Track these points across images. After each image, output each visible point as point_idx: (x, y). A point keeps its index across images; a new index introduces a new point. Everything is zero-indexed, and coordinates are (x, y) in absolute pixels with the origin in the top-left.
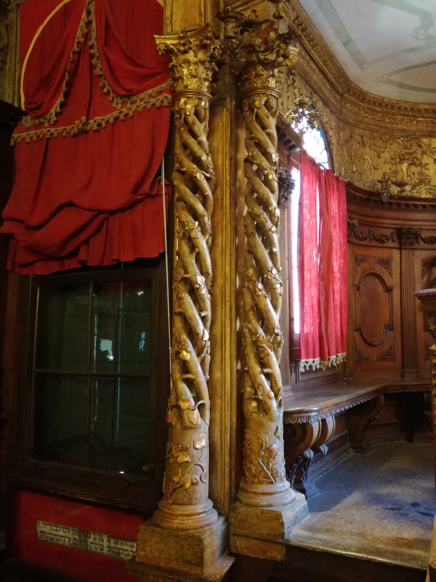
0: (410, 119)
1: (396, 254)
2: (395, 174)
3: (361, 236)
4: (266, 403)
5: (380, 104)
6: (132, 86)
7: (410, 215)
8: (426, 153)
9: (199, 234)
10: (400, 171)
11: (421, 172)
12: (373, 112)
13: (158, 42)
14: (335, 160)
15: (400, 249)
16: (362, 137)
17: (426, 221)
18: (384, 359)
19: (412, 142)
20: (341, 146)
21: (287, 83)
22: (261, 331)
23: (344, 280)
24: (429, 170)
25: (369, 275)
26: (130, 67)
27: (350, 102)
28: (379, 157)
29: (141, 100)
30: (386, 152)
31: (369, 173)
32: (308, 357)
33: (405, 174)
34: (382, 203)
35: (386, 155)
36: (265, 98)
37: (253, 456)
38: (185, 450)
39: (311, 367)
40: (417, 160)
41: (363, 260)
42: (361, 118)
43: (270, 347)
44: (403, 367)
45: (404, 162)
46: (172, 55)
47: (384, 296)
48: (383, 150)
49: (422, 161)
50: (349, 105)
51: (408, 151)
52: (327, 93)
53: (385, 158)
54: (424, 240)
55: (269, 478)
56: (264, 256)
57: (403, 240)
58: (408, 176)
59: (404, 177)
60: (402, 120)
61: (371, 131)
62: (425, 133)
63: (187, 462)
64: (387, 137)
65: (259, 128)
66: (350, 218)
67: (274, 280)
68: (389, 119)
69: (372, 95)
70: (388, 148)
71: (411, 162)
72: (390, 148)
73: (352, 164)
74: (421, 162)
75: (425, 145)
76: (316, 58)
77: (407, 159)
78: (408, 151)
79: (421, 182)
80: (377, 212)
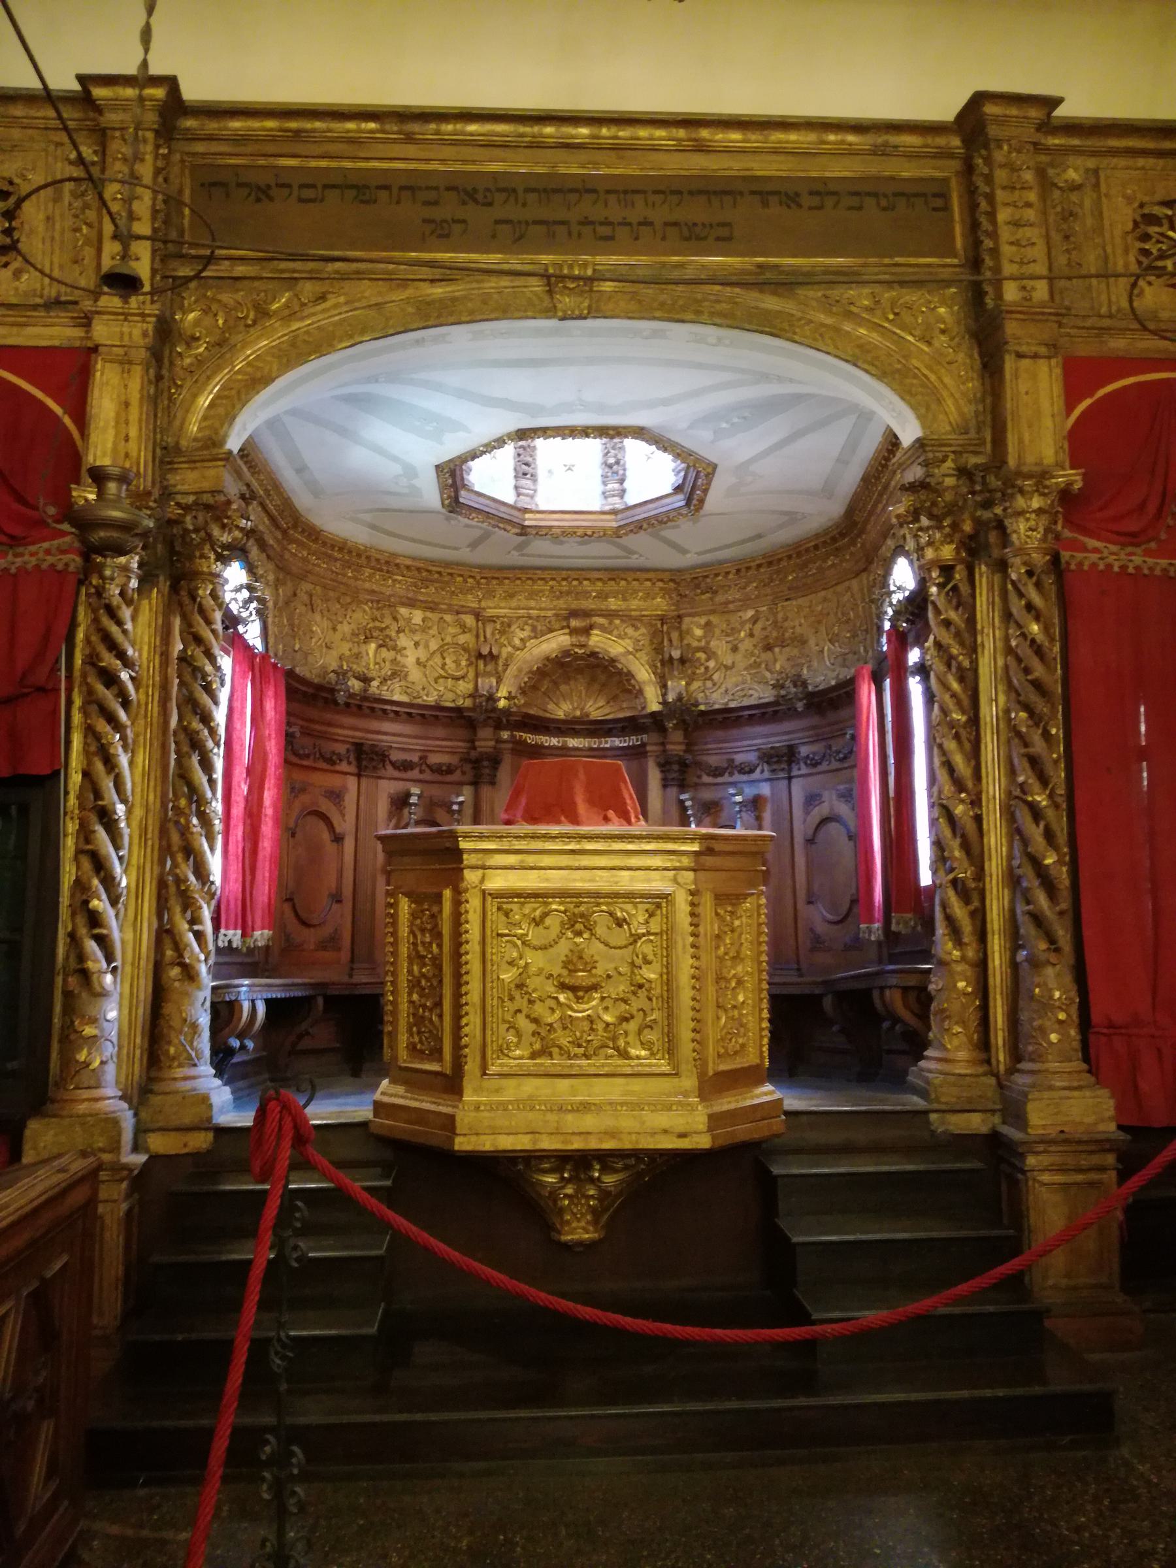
1: (352, 782)
3: (301, 752)
4: (193, 968)
5: (341, 549)
6: (18, 531)
7: (375, 725)
9: (120, 750)
10: (364, 654)
13: (74, 494)
14: (270, 633)
15: (359, 776)
17: (399, 735)
18: (325, 948)
20: (280, 610)
22: (192, 878)
23: (277, 821)
25: (310, 813)
26: (15, 506)
27: (296, 541)
28: (334, 629)
29: (32, 555)
31: (317, 654)
32: (227, 928)
33: (372, 660)
34: (336, 703)
35: (345, 628)
36: (211, 587)
37: (173, 1035)
38: (93, 1021)
41: (303, 790)
42: (310, 567)
43: (203, 898)
44: (352, 961)
47: (330, 848)
51: (377, 624)
54: (393, 764)
55: (192, 1059)
56: (202, 784)
57: (364, 763)
58: (376, 663)
60: (371, 576)
62: (404, 600)
63: (95, 1036)
64: (348, 600)
65: (201, 621)
66: (289, 724)
67: (212, 815)
73: (294, 637)
78: (377, 624)
79: (394, 674)
80: (328, 716)
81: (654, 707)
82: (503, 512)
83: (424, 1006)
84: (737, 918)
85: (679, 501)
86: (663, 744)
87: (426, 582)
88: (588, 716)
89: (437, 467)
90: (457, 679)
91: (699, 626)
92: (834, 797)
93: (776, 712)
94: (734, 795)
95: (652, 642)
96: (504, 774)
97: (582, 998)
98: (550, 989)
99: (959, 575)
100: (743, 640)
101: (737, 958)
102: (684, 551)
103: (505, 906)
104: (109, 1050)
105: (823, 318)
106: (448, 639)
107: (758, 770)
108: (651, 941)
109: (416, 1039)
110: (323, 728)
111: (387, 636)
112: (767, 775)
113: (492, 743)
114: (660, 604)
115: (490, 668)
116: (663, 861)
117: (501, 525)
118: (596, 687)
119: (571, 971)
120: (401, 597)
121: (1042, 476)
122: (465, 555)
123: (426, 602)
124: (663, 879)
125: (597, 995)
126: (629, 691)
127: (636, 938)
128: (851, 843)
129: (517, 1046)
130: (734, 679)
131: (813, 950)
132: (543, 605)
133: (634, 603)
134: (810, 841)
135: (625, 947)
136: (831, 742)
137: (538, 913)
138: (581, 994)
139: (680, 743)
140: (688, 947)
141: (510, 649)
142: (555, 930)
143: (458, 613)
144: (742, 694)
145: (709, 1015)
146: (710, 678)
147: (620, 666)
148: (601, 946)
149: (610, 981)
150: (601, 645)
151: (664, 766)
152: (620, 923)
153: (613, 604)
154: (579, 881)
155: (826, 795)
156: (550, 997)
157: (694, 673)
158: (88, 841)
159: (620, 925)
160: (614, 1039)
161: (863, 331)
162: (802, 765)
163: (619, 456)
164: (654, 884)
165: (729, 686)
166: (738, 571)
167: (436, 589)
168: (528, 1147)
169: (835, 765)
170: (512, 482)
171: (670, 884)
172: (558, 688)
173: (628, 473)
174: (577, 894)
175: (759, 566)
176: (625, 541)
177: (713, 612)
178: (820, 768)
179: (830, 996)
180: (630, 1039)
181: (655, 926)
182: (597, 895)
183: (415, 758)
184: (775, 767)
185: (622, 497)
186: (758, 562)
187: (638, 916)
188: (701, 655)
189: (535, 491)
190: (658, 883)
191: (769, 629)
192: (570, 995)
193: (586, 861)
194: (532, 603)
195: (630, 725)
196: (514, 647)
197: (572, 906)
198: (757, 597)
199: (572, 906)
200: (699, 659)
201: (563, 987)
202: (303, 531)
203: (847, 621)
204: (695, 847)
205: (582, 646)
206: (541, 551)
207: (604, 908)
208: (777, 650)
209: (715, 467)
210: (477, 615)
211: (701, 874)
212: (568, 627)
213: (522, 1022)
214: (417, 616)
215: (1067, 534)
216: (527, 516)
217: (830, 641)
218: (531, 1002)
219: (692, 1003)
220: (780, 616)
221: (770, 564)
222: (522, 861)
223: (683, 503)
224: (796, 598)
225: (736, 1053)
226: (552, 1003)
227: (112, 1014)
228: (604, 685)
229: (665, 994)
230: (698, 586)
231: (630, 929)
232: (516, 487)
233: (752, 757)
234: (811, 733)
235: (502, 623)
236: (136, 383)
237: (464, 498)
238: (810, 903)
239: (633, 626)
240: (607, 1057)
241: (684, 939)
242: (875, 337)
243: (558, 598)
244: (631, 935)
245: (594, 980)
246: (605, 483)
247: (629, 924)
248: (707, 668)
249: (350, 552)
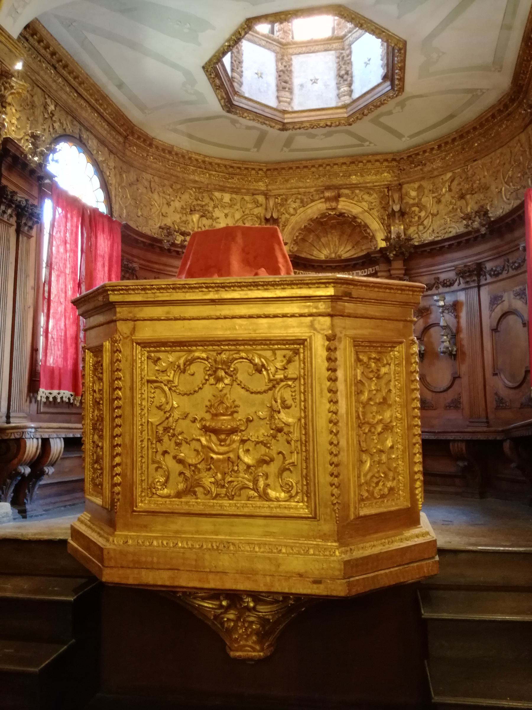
0: (202, 171)
2: (185, 223)
5: (170, 152)
8: (218, 207)
11: (212, 225)
12: (163, 159)
16: (150, 182)
19: (204, 194)
21: (44, 115)
24: (220, 223)
27: (136, 145)
28: (168, 204)
30: (176, 201)
33: (196, 225)
39: (55, 398)
40: (209, 213)
45: (195, 214)
48: (173, 198)
49: (214, 214)
50: (135, 148)
51: (199, 202)
52: (104, 133)
53: (176, 208)
59: (194, 228)
61: (160, 177)
62: (217, 187)
64: (179, 186)
68: (181, 168)
69: (160, 142)
70: (178, 197)
71: (202, 214)
72: (180, 198)
74: (213, 216)
75: (217, 199)
76: (86, 96)
77: (198, 211)
78: (199, 202)
80: (164, 260)
81: (383, 244)
82: (268, 113)
84: (384, 366)
85: (387, 86)
86: (389, 271)
87: (232, 175)
88: (340, 257)
89: (203, 67)
91: (414, 189)
92: (512, 296)
94: (437, 301)
97: (225, 440)
100: (444, 195)
101: (384, 402)
102: (400, 136)
103: (153, 355)
106: (247, 212)
107: (456, 284)
108: (290, 386)
110: (161, 267)
111: (206, 210)
112: (463, 286)
114: (387, 177)
116: (298, 307)
117: (267, 122)
118: (345, 237)
119: (215, 415)
120: (215, 185)
122: (253, 155)
123: (232, 188)
124: (300, 325)
126: (366, 238)
128: (526, 329)
129: (165, 484)
130: (438, 222)
131: (497, 408)
132: (308, 185)
133: (369, 178)
134: (495, 330)
135: (265, 392)
137: (182, 361)
138: (223, 437)
140: (326, 391)
141: (287, 216)
142: (200, 376)
143: (253, 194)
144: (443, 231)
146: (422, 224)
147: (359, 221)
148: (243, 391)
149: (250, 425)
150: (346, 208)
152: (259, 369)
153: (354, 179)
155: (506, 297)
156: (194, 439)
157: (411, 222)
159: (260, 372)
162: (488, 276)
163: (348, 69)
164: (291, 331)
165: (435, 227)
166: (440, 146)
167: (238, 179)
168: (167, 583)
169: (512, 272)
170: (276, 94)
171: (306, 330)
172: (320, 240)
173: (354, 79)
175: (454, 140)
176: (353, 128)
177: (423, 178)
178: (501, 277)
179: (508, 441)
180: (270, 481)
181: (293, 371)
182: (236, 342)
184: (468, 279)
185: (350, 96)
186: (453, 137)
188: (416, 209)
189: (291, 99)
191: (462, 184)
192: (214, 437)
193: (226, 310)
194: (301, 184)
196: (289, 214)
197: (214, 354)
198: (453, 162)
199: (214, 354)
200: (414, 212)
201: (206, 430)
202: (139, 138)
203: (518, 166)
204: (330, 291)
205: (334, 209)
207: (243, 355)
208: (468, 197)
209: (405, 43)
211: (338, 321)
212: (324, 197)
213: (169, 462)
214: (227, 197)
216: (286, 116)
217: (506, 183)
218: (178, 444)
219: (330, 447)
220: (470, 173)
221: (461, 137)
222: (168, 313)
223: (390, 88)
224: (480, 159)
225: (383, 496)
228: (350, 236)
229: (303, 438)
230: (412, 163)
231: (268, 374)
232: (278, 97)
233: (451, 275)
234: (494, 252)
235: (282, 199)
237: (237, 101)
238: (495, 374)
239: (368, 193)
240: (249, 498)
241: (321, 384)
243: (317, 179)
244: (270, 380)
246: (339, 88)
247: (267, 370)
248: (419, 217)
249: (177, 154)
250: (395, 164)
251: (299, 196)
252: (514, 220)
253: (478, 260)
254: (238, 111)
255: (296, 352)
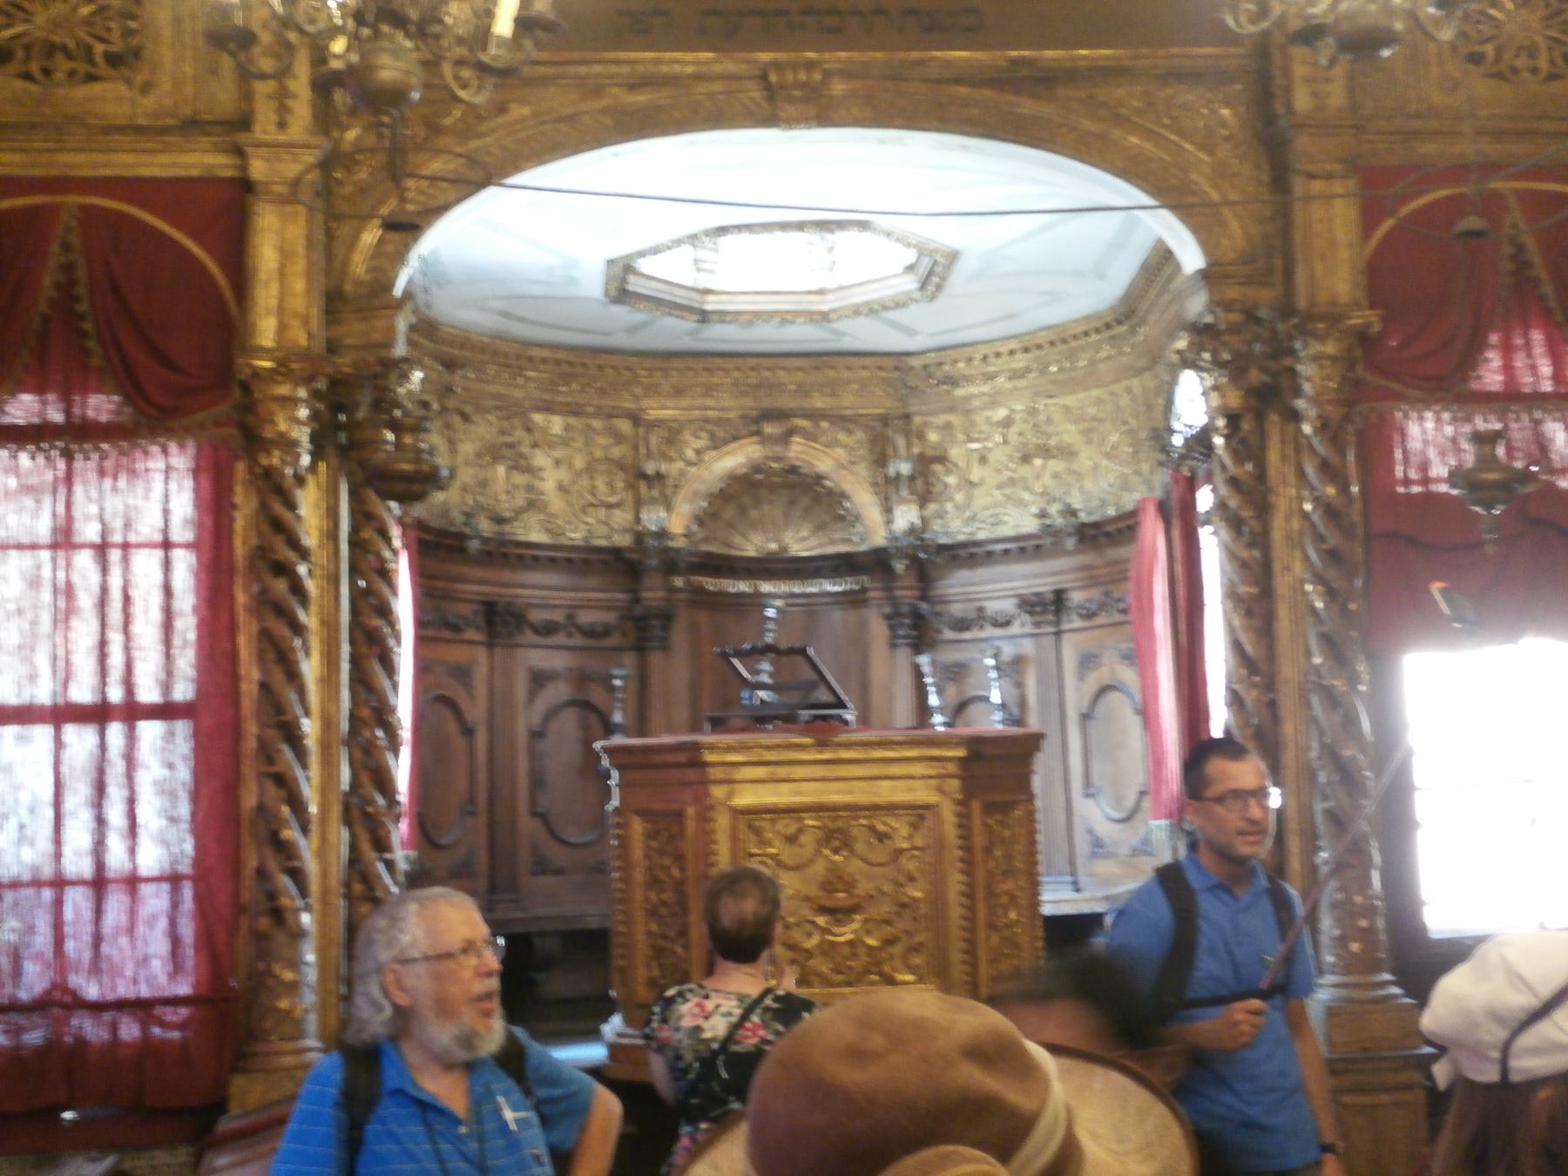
1: (481, 654)
7: (508, 576)
15: (490, 645)
38: (123, 866)
46: (252, 361)
47: (459, 742)
54: (536, 630)
79: (531, 505)
83: (664, 937)
85: (910, 284)
87: (566, 378)
90: (609, 506)
93: (1038, 547)
95: (871, 452)
96: (679, 636)
98: (807, 912)
99: (1246, 425)
104: (309, 998)
105: (1090, 125)
106: (599, 453)
108: (915, 857)
109: (656, 972)
112: (1029, 629)
113: (661, 594)
115: (655, 493)
121: (1334, 318)
123: (568, 404)
125: (857, 917)
127: (899, 852)
136: (1111, 587)
139: (912, 588)
143: (611, 416)
145: (982, 933)
151: (892, 619)
152: (882, 837)
153: (819, 402)
154: (835, 795)
158: (270, 761)
160: (878, 963)
161: (1134, 140)
162: (1075, 617)
174: (833, 808)
182: (854, 808)
183: (558, 616)
184: (1039, 618)
187: (900, 828)
190: (923, 794)
194: (709, 402)
195: (844, 565)
201: (823, 910)
204: (960, 753)
205: (778, 459)
206: (721, 336)
210: (636, 419)
214: (556, 424)
215: (1370, 378)
216: (711, 298)
226: (808, 927)
227: (310, 957)
233: (1008, 606)
236: (297, 231)
242: (1148, 147)
245: (856, 901)
250: (896, 375)
251: (709, 427)
252: (1119, 531)
253: (1060, 583)
254: (720, 395)
255: (922, 818)
